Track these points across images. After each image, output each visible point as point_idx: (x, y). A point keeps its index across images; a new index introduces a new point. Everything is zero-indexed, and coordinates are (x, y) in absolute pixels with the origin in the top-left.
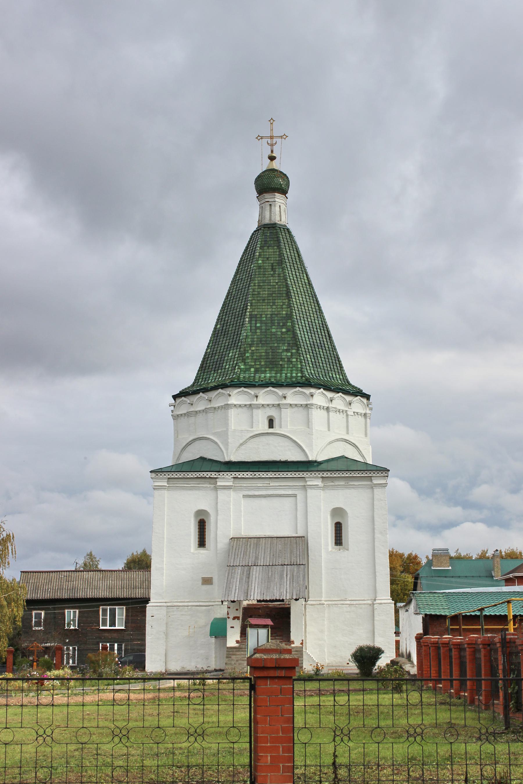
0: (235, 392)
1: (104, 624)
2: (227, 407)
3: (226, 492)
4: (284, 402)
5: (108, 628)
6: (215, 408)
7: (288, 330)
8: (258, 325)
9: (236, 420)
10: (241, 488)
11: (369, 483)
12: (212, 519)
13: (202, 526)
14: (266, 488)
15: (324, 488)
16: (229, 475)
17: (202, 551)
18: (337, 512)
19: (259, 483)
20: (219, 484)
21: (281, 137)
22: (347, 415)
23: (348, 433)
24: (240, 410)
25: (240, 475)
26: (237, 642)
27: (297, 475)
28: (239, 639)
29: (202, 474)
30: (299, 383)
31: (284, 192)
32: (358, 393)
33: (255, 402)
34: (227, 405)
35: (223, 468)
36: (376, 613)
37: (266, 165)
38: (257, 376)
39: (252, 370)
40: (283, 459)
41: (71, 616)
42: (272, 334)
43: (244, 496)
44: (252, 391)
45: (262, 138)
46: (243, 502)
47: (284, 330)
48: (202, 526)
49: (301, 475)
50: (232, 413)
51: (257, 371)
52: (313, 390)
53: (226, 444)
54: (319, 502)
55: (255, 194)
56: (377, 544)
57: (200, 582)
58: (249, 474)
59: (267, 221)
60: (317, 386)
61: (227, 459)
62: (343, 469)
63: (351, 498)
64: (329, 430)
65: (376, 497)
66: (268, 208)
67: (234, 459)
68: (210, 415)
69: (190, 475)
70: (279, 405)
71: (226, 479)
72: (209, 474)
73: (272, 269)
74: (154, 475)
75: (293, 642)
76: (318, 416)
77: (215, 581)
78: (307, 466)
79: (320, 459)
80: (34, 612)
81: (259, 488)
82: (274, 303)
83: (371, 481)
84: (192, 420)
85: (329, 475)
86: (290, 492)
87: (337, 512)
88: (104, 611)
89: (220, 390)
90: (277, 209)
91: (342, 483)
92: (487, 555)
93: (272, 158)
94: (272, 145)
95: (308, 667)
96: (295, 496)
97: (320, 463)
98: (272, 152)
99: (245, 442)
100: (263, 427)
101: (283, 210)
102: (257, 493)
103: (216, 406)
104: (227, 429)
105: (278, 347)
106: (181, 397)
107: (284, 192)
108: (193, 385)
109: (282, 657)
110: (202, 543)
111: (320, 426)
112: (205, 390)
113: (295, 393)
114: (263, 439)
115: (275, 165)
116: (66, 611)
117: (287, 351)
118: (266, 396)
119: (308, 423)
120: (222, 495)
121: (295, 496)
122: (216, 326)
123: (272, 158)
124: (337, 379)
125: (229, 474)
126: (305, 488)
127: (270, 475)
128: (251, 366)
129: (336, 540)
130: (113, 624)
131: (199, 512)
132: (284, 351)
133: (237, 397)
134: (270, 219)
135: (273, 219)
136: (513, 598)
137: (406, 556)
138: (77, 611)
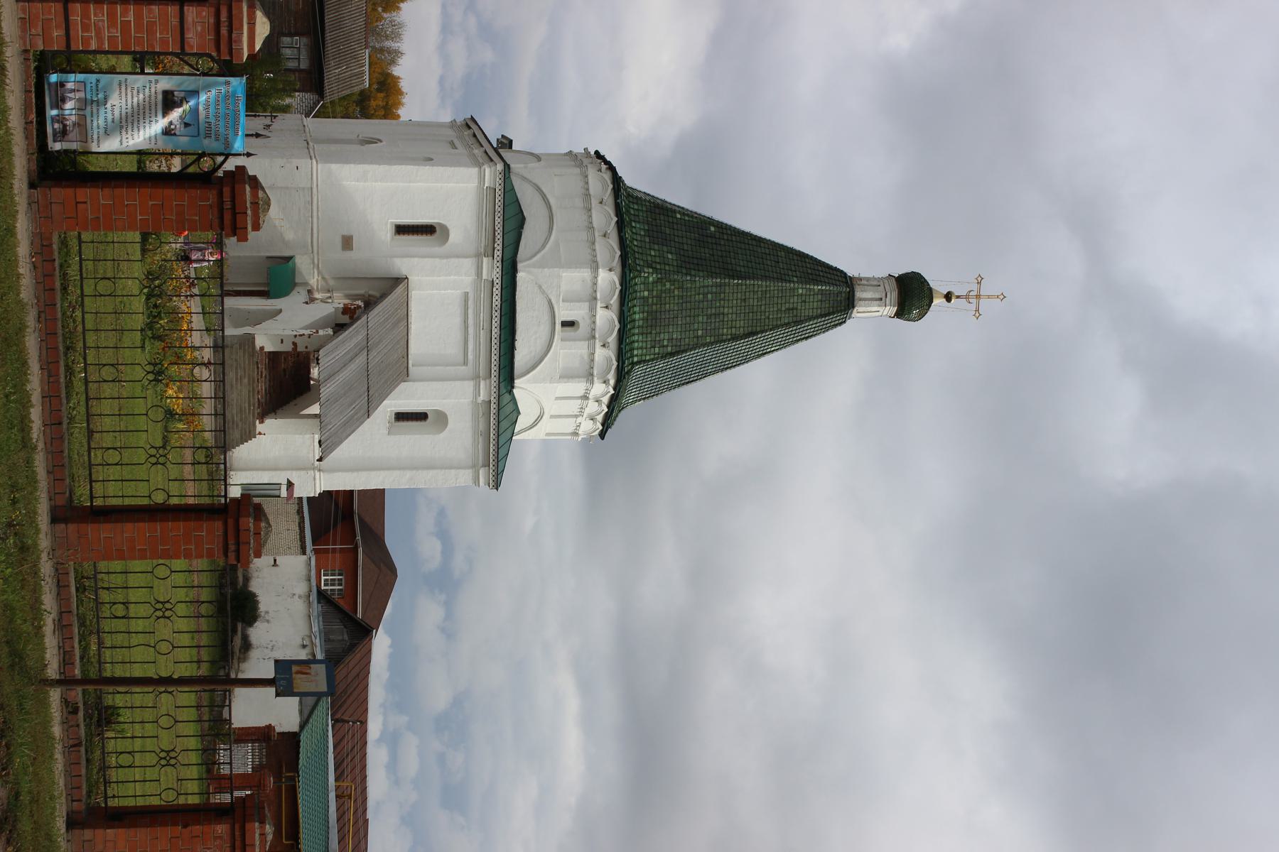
0: (615, 277)
2: (595, 266)
3: (473, 271)
4: (598, 344)
6: (593, 243)
9: (573, 279)
11: (480, 463)
12: (437, 250)
14: (477, 325)
15: (475, 403)
16: (496, 274)
17: (387, 233)
19: (484, 316)
20: (485, 260)
22: (576, 416)
23: (552, 417)
24: (589, 283)
25: (497, 291)
26: (262, 348)
27: (494, 368)
28: (266, 350)
29: (499, 236)
31: (899, 314)
33: (599, 305)
34: (597, 268)
35: (508, 255)
36: (303, 473)
40: (517, 344)
43: (466, 294)
44: (615, 300)
46: (458, 293)
49: (494, 373)
50: (586, 274)
52: (612, 382)
53: (541, 265)
54: (458, 399)
56: (397, 473)
57: (346, 233)
58: (498, 303)
61: (520, 266)
62: (500, 420)
63: (459, 437)
64: (557, 398)
65: (462, 471)
66: (878, 296)
67: (521, 276)
68: (584, 235)
69: (498, 220)
70: (594, 337)
71: (492, 270)
72: (500, 248)
75: (262, 422)
76: (578, 387)
77: (348, 254)
78: (507, 375)
79: (515, 391)
81: (477, 315)
83: (484, 466)
84: (579, 202)
85: (493, 411)
86: (471, 357)
87: (442, 419)
89: (619, 253)
91: (482, 427)
93: (948, 297)
94: (967, 297)
96: (465, 363)
97: (511, 392)
98: (958, 297)
99: (543, 292)
100: (563, 314)
101: (872, 315)
102: (470, 311)
103: (597, 247)
104: (561, 266)
106: (613, 183)
107: (899, 314)
110: (402, 230)
111: (559, 400)
113: (609, 360)
114: (546, 318)
115: (938, 301)
118: (606, 318)
119: (567, 376)
120: (468, 264)
121: (465, 363)
123: (948, 297)
125: (499, 276)
126: (476, 378)
127: (496, 332)
131: (445, 231)
133: (608, 279)
134: (861, 299)
135: (862, 303)
137: (394, 45)
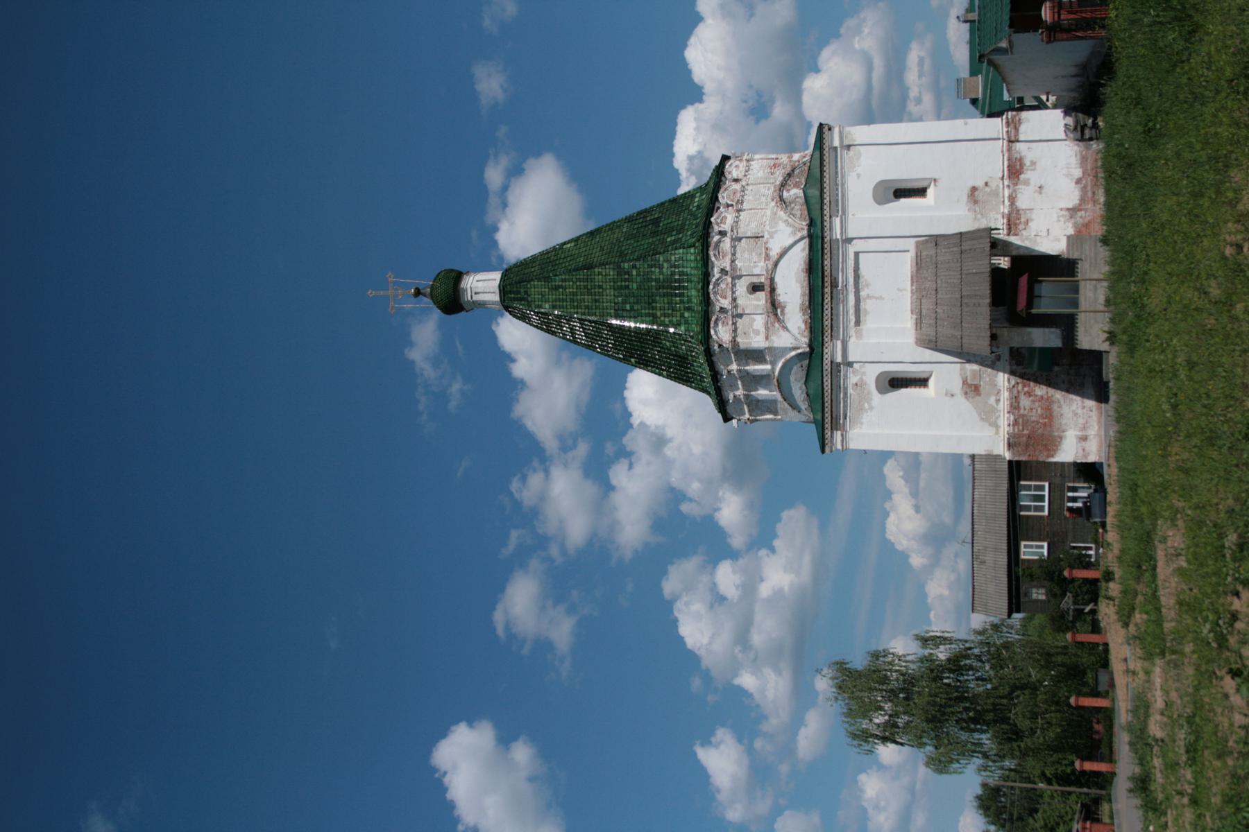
1: (1041, 509)
5: (1046, 504)
7: (634, 267)
8: (628, 307)
10: (846, 329)
13: (896, 382)
20: (839, 359)
30: (703, 288)
32: (719, 172)
41: (1034, 550)
42: (639, 288)
43: (858, 323)
47: (634, 272)
48: (896, 382)
54: (861, 216)
55: (463, 313)
60: (708, 225)
74: (827, 449)
82: (600, 287)
90: (480, 284)
92: (946, 593)
95: (1137, 770)
96: (857, 254)
105: (657, 280)
108: (708, 393)
110: (922, 382)
116: (1023, 557)
117: (661, 267)
123: (418, 293)
128: (682, 315)
129: (920, 386)
132: (661, 273)
138: (1023, 543)
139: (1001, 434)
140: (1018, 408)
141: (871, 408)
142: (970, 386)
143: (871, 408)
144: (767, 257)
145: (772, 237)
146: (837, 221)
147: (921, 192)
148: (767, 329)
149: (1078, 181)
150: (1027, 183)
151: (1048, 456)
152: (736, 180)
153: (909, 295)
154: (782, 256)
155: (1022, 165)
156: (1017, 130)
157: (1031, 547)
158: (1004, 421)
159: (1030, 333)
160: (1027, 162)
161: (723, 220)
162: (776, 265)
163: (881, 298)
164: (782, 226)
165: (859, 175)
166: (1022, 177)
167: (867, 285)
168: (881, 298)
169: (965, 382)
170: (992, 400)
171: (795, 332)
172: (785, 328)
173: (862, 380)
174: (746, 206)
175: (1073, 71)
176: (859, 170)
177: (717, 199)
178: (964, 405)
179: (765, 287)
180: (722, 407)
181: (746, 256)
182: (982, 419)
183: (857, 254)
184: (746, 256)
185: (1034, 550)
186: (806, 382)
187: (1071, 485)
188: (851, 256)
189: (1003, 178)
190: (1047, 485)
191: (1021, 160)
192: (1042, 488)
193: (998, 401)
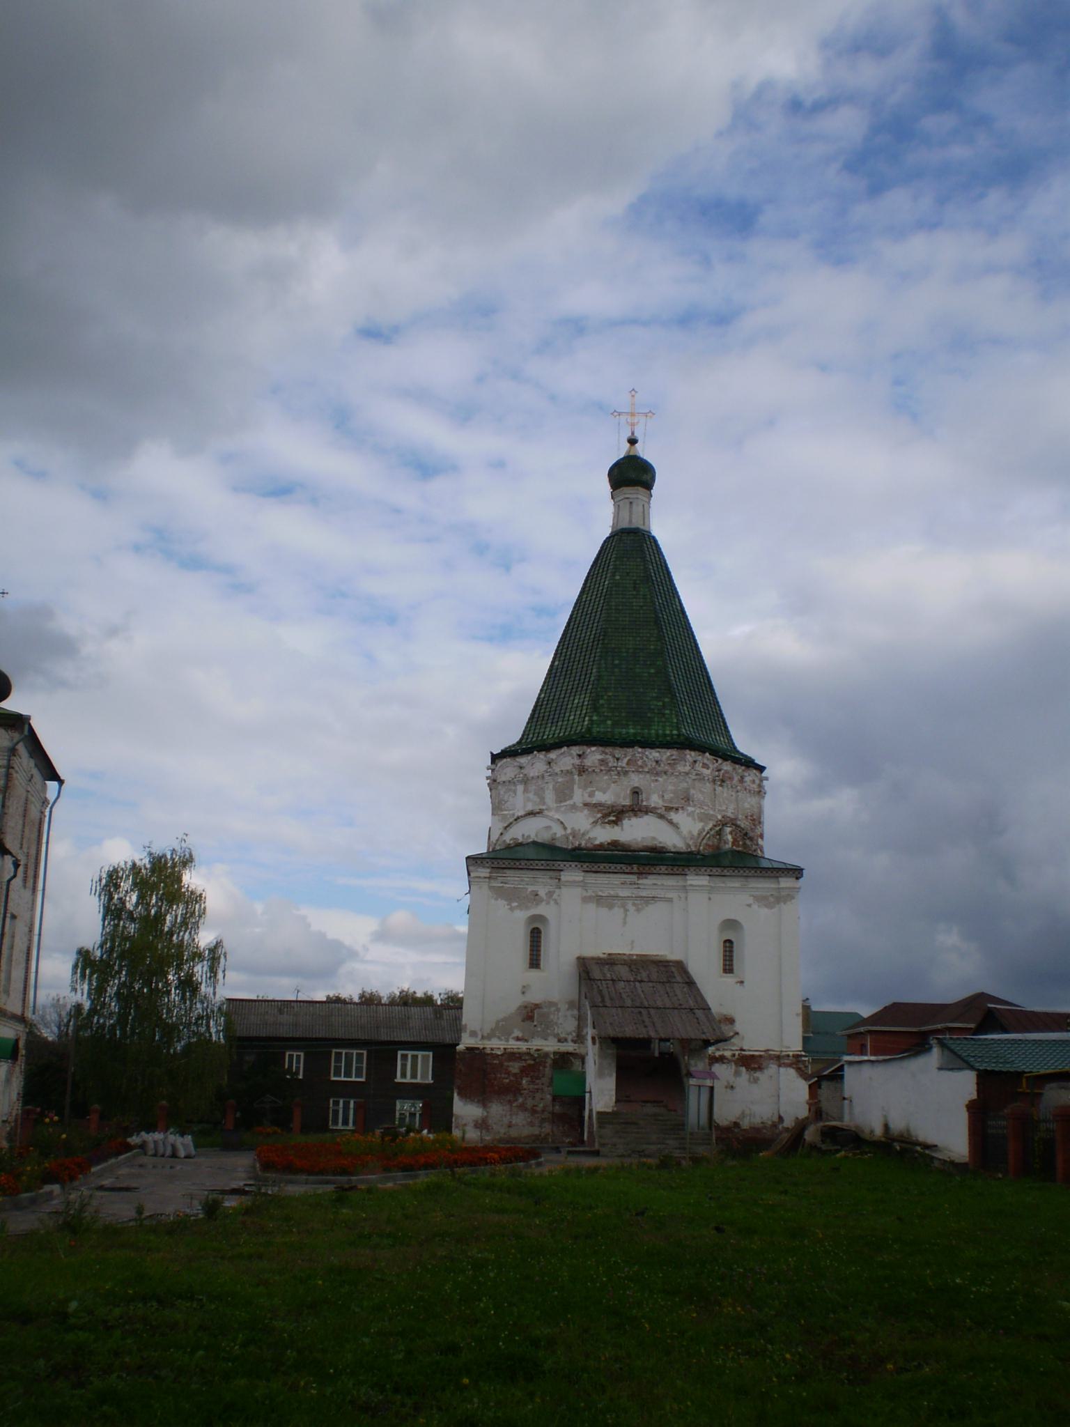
1: (338, 1073)
13: (535, 937)
17: (534, 973)
18: (731, 924)
21: (646, 415)
37: (622, 450)
38: (617, 731)
39: (609, 722)
45: (620, 414)
48: (535, 937)
51: (615, 724)
59: (625, 524)
73: (635, 588)
80: (400, 1053)
88: (404, 1057)
96: (670, 900)
108: (519, 743)
109: (24, 1052)
112: (545, 747)
122: (553, 662)
123: (633, 442)
124: (721, 742)
130: (414, 1076)
134: (630, 521)
136: (17, 1069)
139: (486, 1042)
140: (510, 1060)
141: (512, 909)
142: (532, 1011)
143: (512, 909)
144: (669, 809)
145: (689, 815)
146: (737, 885)
147: (728, 968)
148: (595, 805)
149: (736, 1124)
150: (737, 1074)
151: (459, 1088)
152: (742, 780)
153: (627, 952)
154: (670, 822)
155: (755, 1069)
156: (790, 1065)
157: (298, 1062)
158: (497, 1045)
159: (611, 1076)
160: (758, 1074)
161: (705, 766)
162: (661, 817)
163: (625, 923)
164: (700, 825)
165: (749, 905)
166: (743, 1069)
167: (638, 910)
168: (625, 923)
169: (537, 1006)
170: (517, 1033)
171: (591, 835)
172: (595, 823)
173: (542, 900)
174: (719, 789)
175: (897, 1125)
176: (755, 907)
177: (725, 760)
178: (513, 1004)
179: (637, 808)
180: (508, 753)
181: (671, 788)
182: (498, 1022)
183: (670, 900)
184: (671, 788)
185: (296, 1061)
186: (534, 843)
187: (352, 1105)
188: (669, 895)
189: (742, 1050)
190: (363, 1080)
191: (760, 1068)
192: (358, 1075)
193: (518, 1039)
